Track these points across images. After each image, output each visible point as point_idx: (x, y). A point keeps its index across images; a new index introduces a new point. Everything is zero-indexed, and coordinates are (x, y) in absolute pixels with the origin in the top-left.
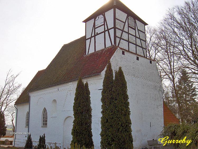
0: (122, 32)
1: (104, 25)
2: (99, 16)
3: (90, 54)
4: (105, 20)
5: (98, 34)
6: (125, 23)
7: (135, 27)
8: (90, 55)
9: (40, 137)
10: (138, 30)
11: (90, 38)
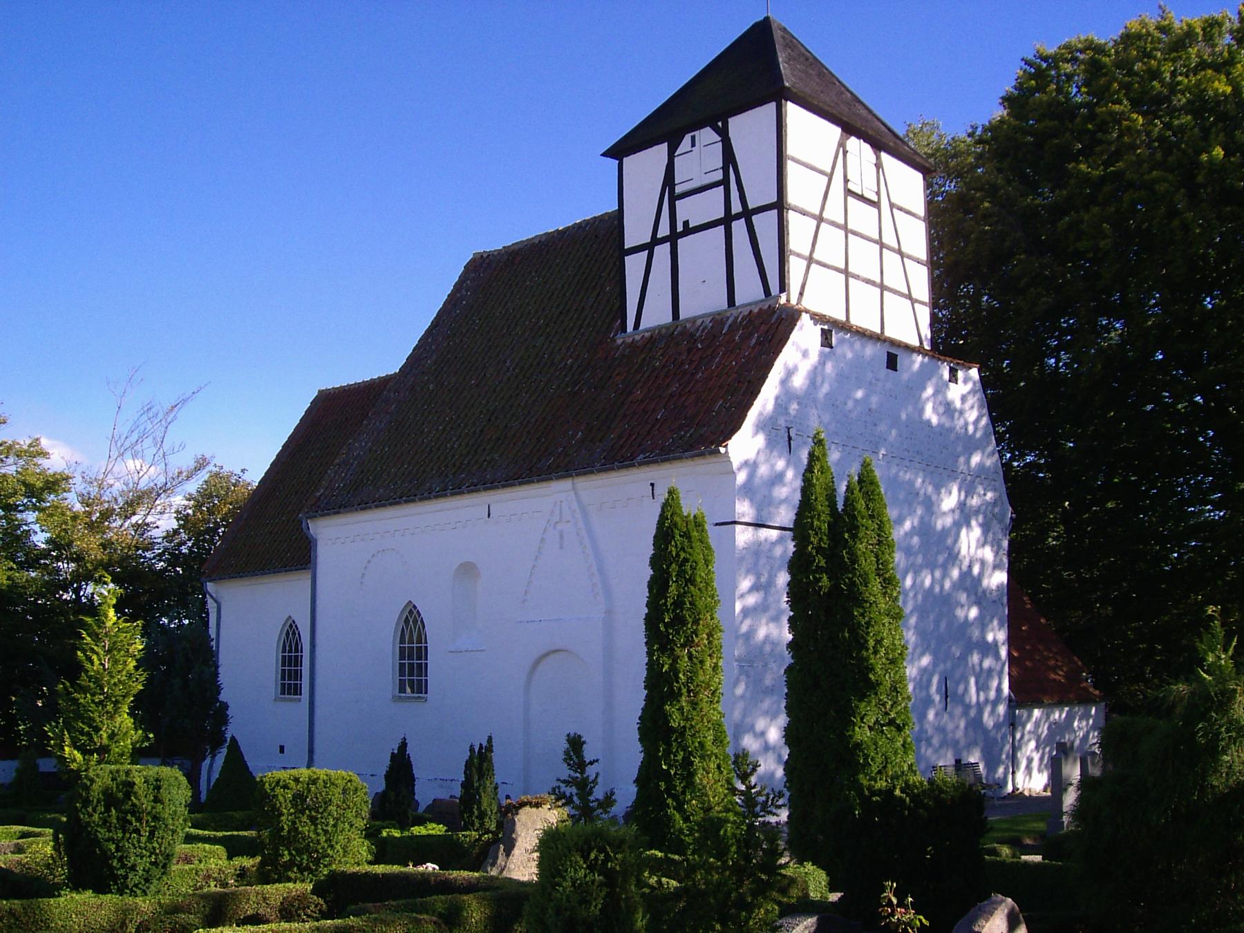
0: (715, 185)
1: (725, 182)
2: (696, 133)
3: (647, 330)
4: (729, 158)
5: (688, 230)
6: (830, 177)
7: (878, 193)
8: (647, 335)
9: (472, 749)
10: (892, 206)
11: (649, 247)
